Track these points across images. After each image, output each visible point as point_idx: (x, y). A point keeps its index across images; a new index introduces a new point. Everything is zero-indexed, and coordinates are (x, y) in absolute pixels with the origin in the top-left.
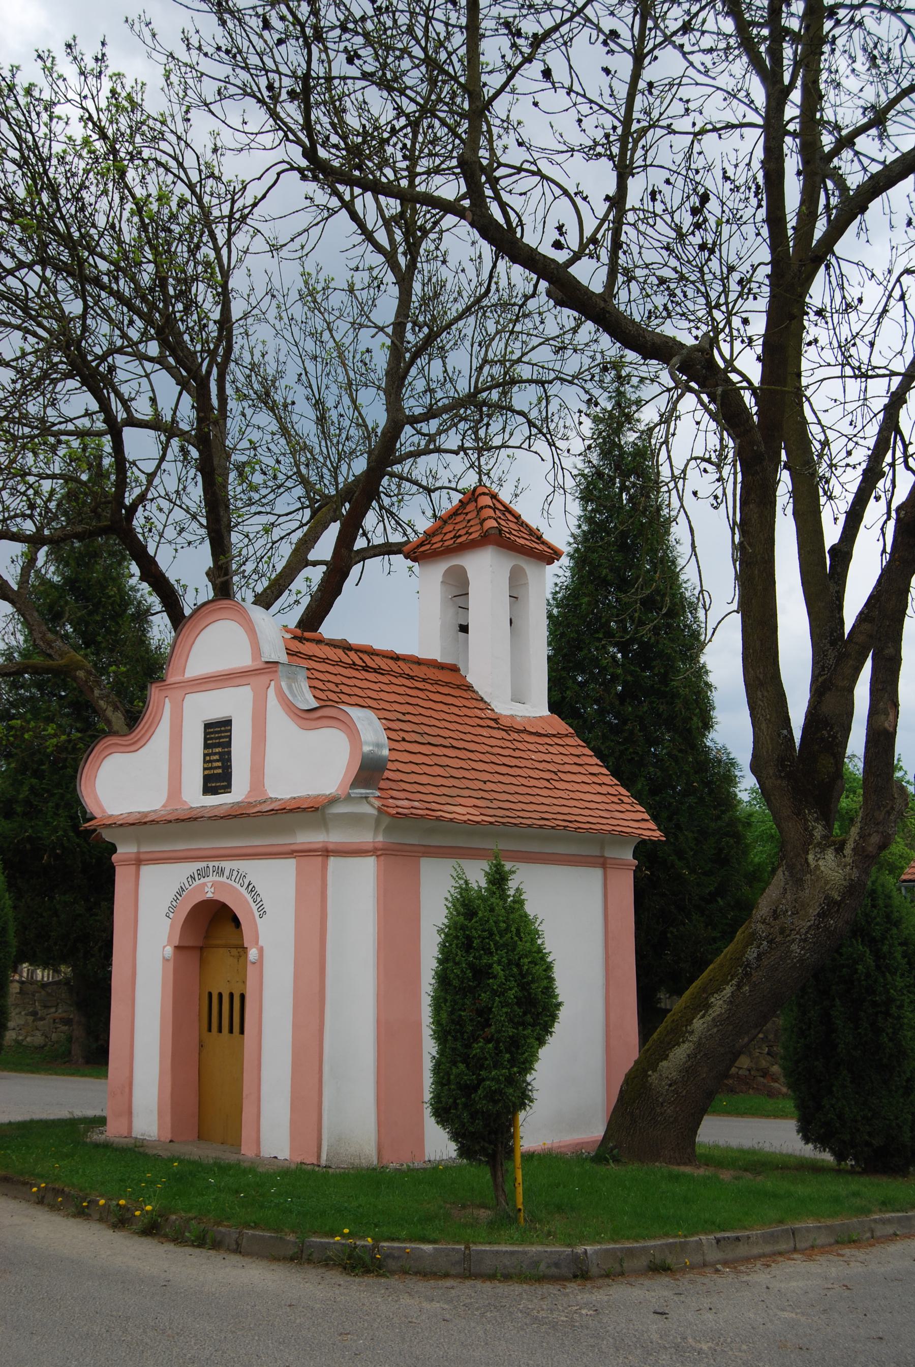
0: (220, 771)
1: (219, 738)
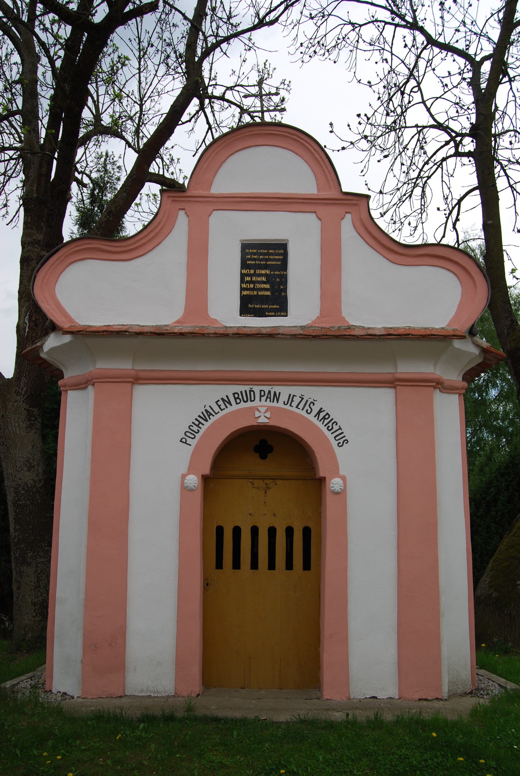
0: (268, 293)
1: (267, 260)
